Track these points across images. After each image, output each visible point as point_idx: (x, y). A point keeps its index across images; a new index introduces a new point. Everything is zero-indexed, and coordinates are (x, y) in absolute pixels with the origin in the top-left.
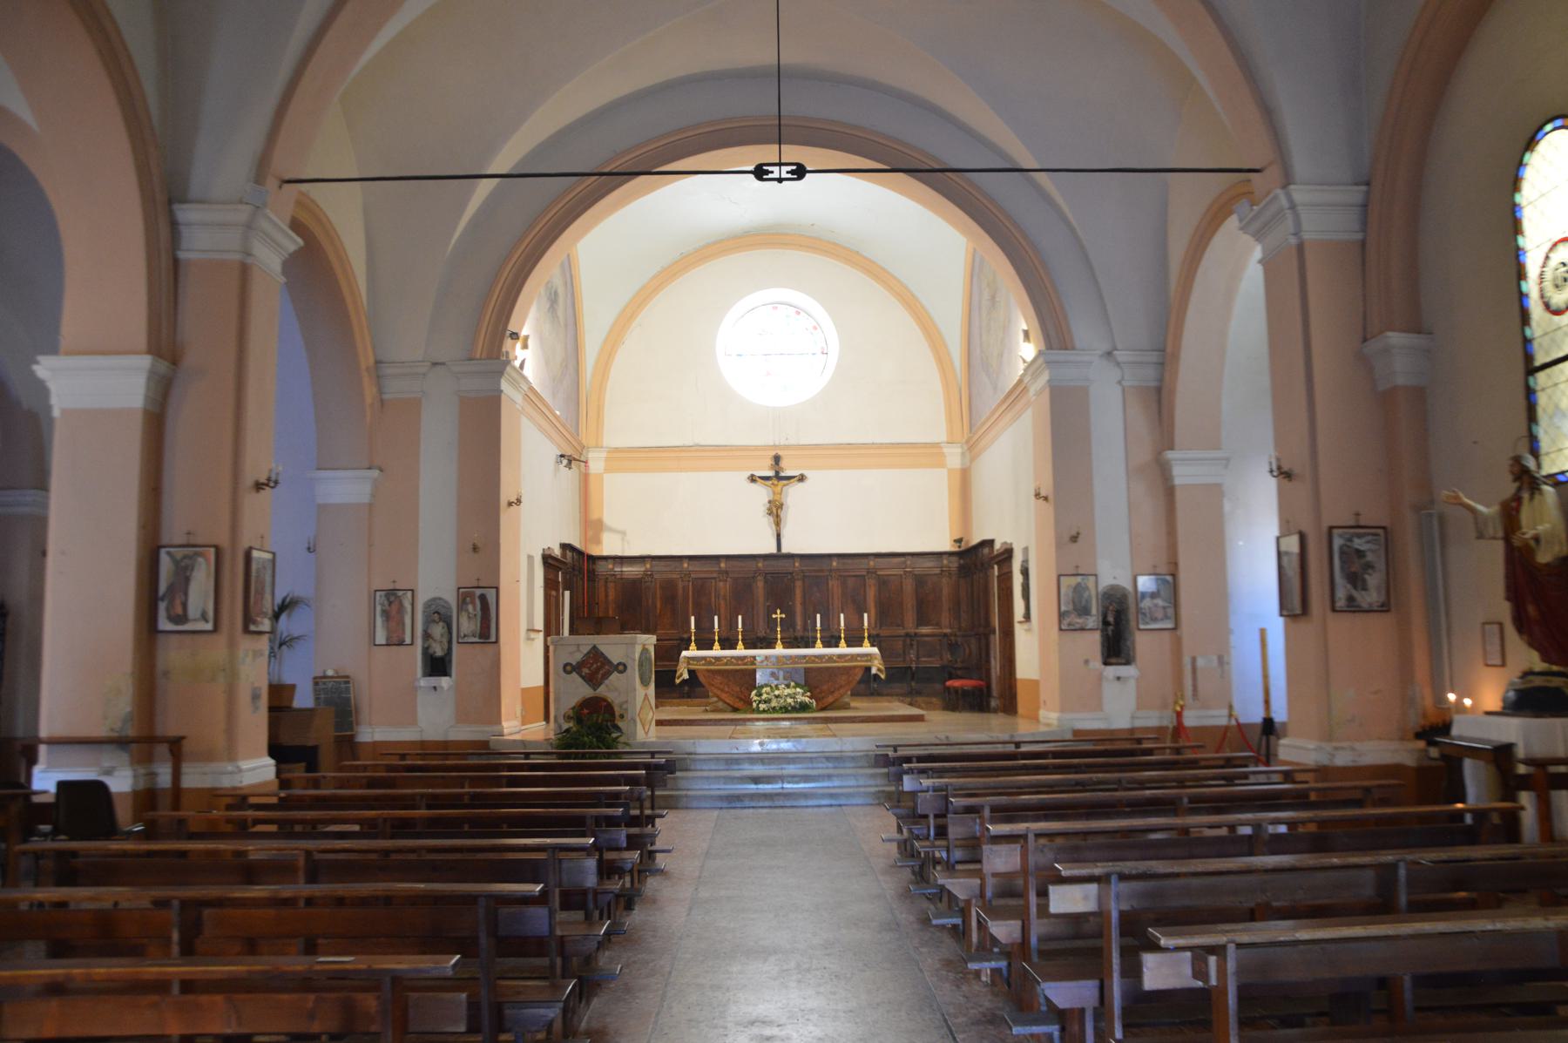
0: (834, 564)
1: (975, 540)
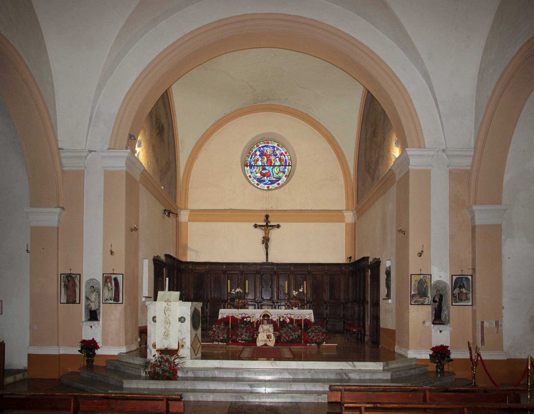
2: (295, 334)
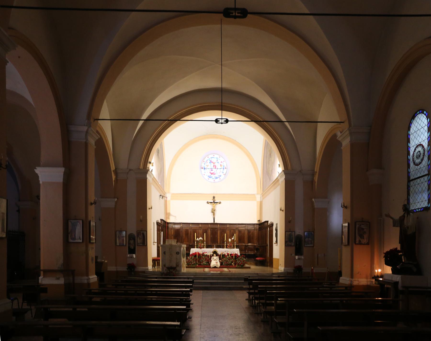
0: (228, 226)
1: (263, 221)
2: (230, 261)
